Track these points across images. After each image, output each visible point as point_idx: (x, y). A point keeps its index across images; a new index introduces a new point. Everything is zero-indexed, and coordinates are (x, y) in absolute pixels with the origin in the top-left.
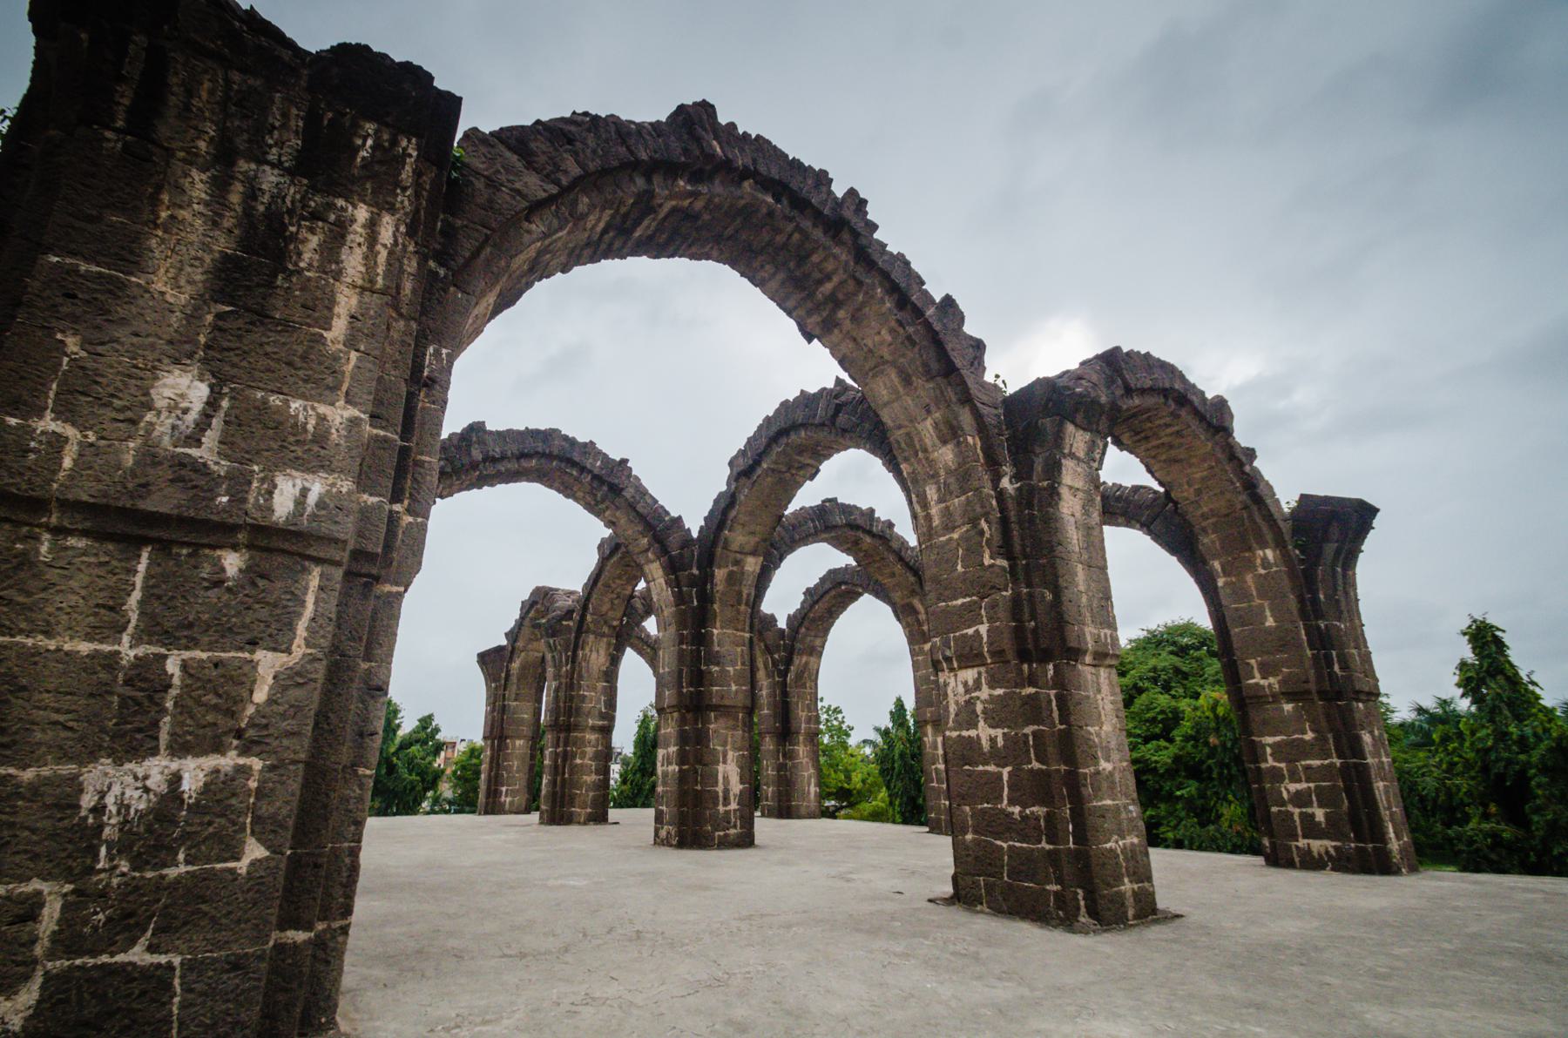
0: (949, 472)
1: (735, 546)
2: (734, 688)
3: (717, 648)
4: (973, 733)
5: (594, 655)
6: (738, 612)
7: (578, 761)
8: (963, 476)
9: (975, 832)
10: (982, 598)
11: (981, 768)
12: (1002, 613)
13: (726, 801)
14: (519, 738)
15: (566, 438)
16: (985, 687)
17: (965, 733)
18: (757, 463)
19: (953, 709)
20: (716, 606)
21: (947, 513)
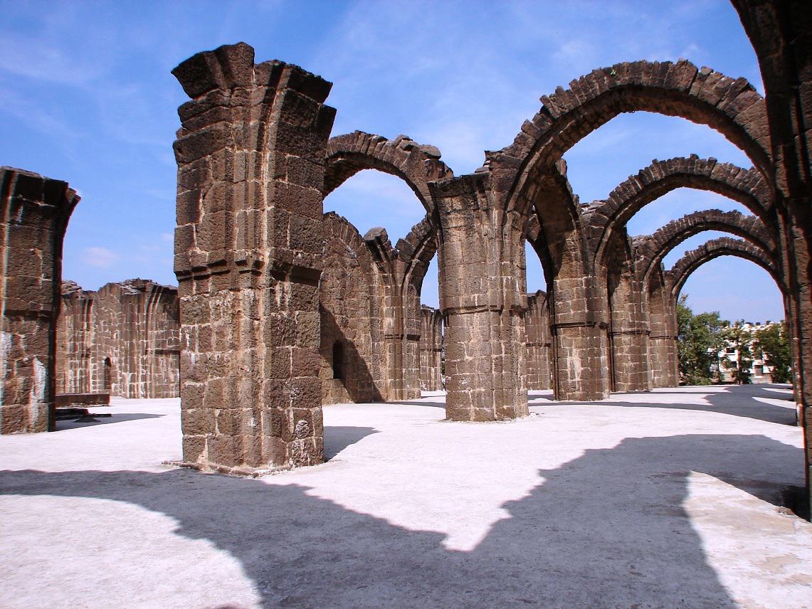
2: (572, 312)
6: (571, 266)
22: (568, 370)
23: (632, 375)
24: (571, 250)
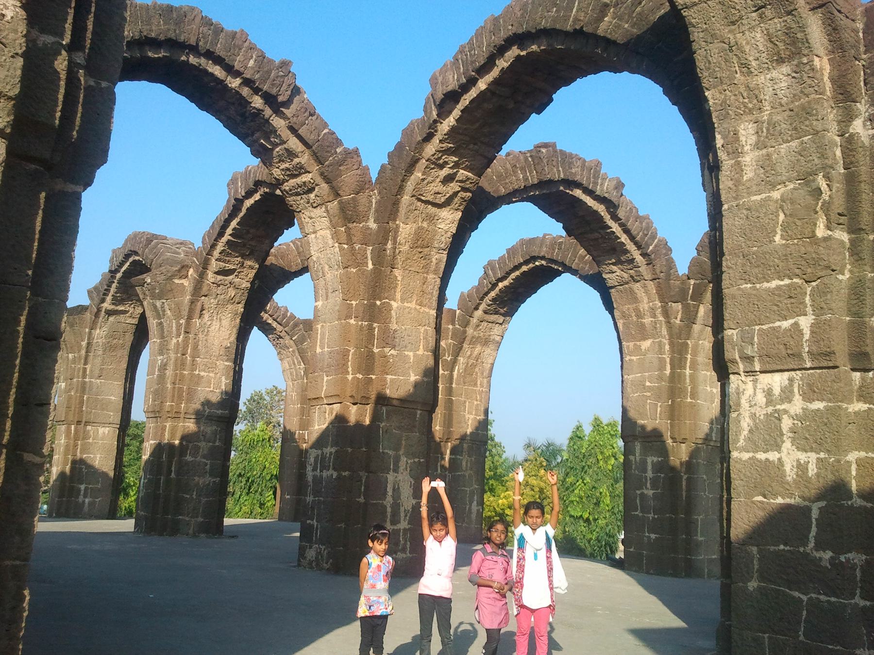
0: (777, 105)
4: (773, 456)
5: (215, 325)
7: (189, 458)
8: (801, 116)
9: (762, 578)
12: (839, 301)
13: (395, 521)
14: (104, 424)
15: (207, 22)
17: (761, 456)
20: (396, 272)
21: (766, 165)
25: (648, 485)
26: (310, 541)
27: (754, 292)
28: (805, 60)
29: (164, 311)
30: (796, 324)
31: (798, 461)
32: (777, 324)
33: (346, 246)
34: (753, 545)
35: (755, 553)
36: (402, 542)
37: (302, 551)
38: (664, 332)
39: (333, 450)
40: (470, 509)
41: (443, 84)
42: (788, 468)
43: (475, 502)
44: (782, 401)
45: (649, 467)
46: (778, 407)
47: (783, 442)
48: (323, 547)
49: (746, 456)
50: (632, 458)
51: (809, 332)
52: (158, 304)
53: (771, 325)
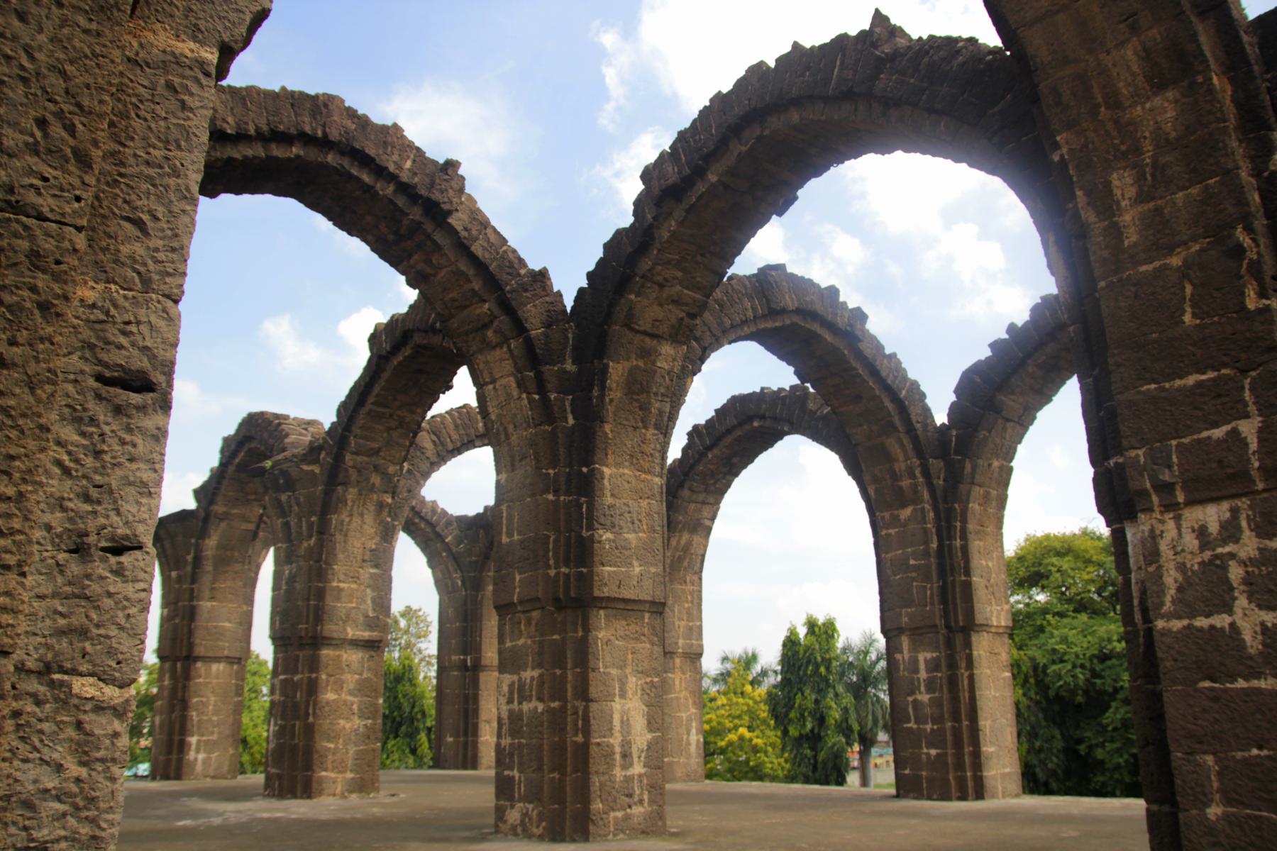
0: (1162, 142)
1: (645, 325)
3: (609, 500)
4: (1221, 621)
9: (1228, 800)
10: (1244, 372)
11: (1241, 684)
13: (627, 764)
16: (1248, 535)
17: (1201, 622)
18: (699, 172)
19: (1171, 579)
22: (616, 741)
23: (357, 753)
24: (656, 394)
25: (922, 689)
26: (511, 798)
27: (1163, 394)
28: (1200, 79)
29: (291, 507)
30: (1235, 433)
31: (1263, 624)
32: (1205, 434)
33: (537, 397)
34: (1205, 753)
35: (1211, 763)
36: (637, 792)
37: (500, 813)
38: (926, 496)
39: (536, 673)
40: (688, 739)
41: (659, 179)
42: (1247, 636)
43: (694, 731)
44: (1224, 542)
45: (922, 666)
46: (1220, 550)
47: (1235, 599)
48: (530, 806)
49: (1177, 625)
50: (898, 656)
51: (1255, 440)
52: (284, 497)
53: (1195, 437)
